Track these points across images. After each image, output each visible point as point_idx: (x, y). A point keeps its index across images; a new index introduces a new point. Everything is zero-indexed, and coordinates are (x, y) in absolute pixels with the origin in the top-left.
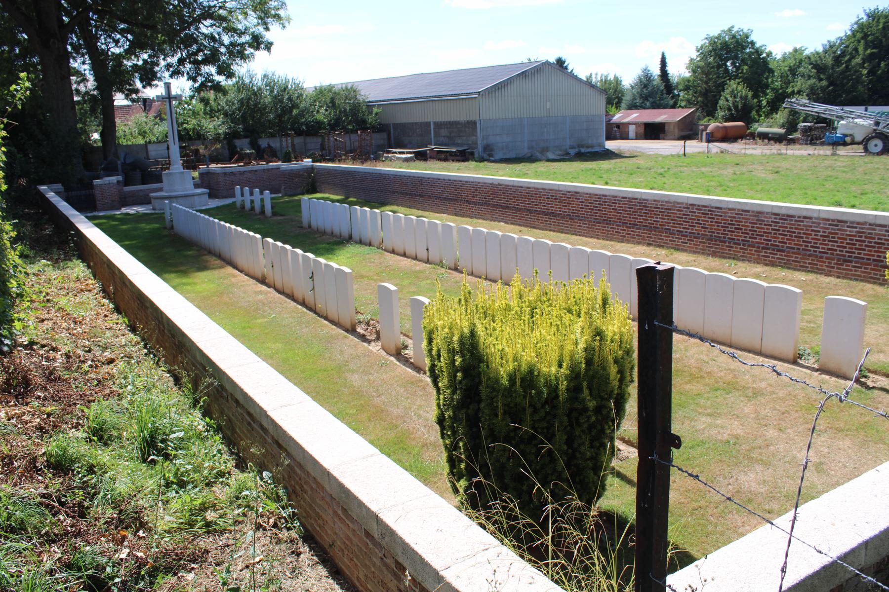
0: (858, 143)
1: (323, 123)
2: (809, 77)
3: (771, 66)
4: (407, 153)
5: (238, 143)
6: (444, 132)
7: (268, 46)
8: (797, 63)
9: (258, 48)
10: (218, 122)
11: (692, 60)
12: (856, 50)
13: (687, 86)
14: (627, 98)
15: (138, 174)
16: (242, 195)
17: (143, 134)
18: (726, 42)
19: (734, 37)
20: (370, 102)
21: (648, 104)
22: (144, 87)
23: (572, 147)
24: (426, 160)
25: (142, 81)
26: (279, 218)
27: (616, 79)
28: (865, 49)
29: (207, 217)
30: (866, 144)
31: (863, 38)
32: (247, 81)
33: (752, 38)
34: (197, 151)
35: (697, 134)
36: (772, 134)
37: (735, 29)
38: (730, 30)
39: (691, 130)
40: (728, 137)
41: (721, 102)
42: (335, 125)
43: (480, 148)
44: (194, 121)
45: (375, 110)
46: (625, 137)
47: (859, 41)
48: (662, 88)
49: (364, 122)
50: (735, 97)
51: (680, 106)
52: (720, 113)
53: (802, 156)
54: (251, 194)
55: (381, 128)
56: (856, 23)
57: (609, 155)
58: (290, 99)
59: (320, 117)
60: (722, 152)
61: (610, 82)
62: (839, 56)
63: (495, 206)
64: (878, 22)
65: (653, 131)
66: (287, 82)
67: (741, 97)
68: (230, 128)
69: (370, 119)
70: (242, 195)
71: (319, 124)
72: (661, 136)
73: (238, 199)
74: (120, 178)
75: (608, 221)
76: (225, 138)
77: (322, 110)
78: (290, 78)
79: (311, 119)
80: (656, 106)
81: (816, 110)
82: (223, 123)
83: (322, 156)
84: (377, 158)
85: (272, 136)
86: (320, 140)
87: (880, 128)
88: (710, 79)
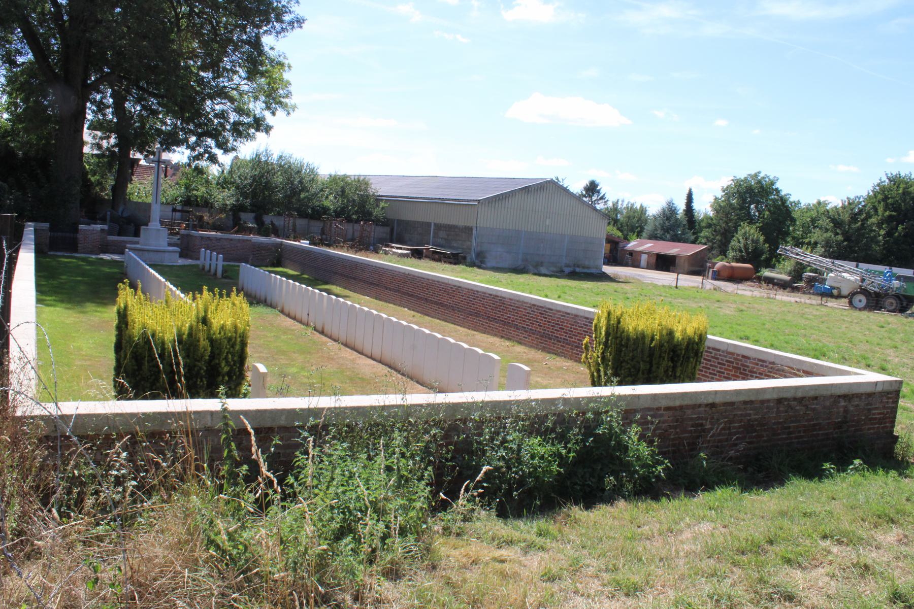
0: (845, 297)
1: (329, 209)
2: (827, 230)
3: (794, 215)
4: (405, 249)
5: (243, 216)
6: (442, 234)
7: (268, 129)
8: (820, 215)
9: (258, 130)
10: (226, 193)
11: (716, 199)
12: (876, 210)
14: (648, 228)
18: (751, 186)
19: (759, 182)
21: (668, 236)
23: (568, 266)
24: (420, 258)
27: (641, 206)
28: (885, 211)
30: (851, 298)
31: (883, 200)
32: (263, 159)
33: (778, 185)
34: (202, 217)
35: (704, 271)
36: (778, 279)
37: (762, 175)
38: (756, 175)
40: (734, 277)
41: (733, 243)
42: (339, 213)
43: (473, 253)
46: (636, 265)
47: (879, 202)
48: (685, 222)
49: (370, 214)
50: (746, 239)
51: (700, 243)
52: (731, 254)
53: (790, 302)
55: (386, 222)
56: (878, 185)
57: (604, 277)
58: (301, 182)
59: (327, 203)
60: (715, 289)
61: (635, 211)
62: (856, 214)
63: (404, 293)
64: (898, 187)
65: (664, 263)
66: (302, 166)
67: (753, 241)
68: (238, 200)
69: (376, 212)
71: (325, 210)
74: (106, 227)
75: (477, 315)
76: (230, 210)
77: (331, 197)
78: (305, 162)
79: (317, 204)
80: (676, 239)
81: (807, 259)
83: (321, 240)
84: (376, 251)
85: (279, 214)
86: (322, 225)
87: (864, 284)
88: (731, 220)
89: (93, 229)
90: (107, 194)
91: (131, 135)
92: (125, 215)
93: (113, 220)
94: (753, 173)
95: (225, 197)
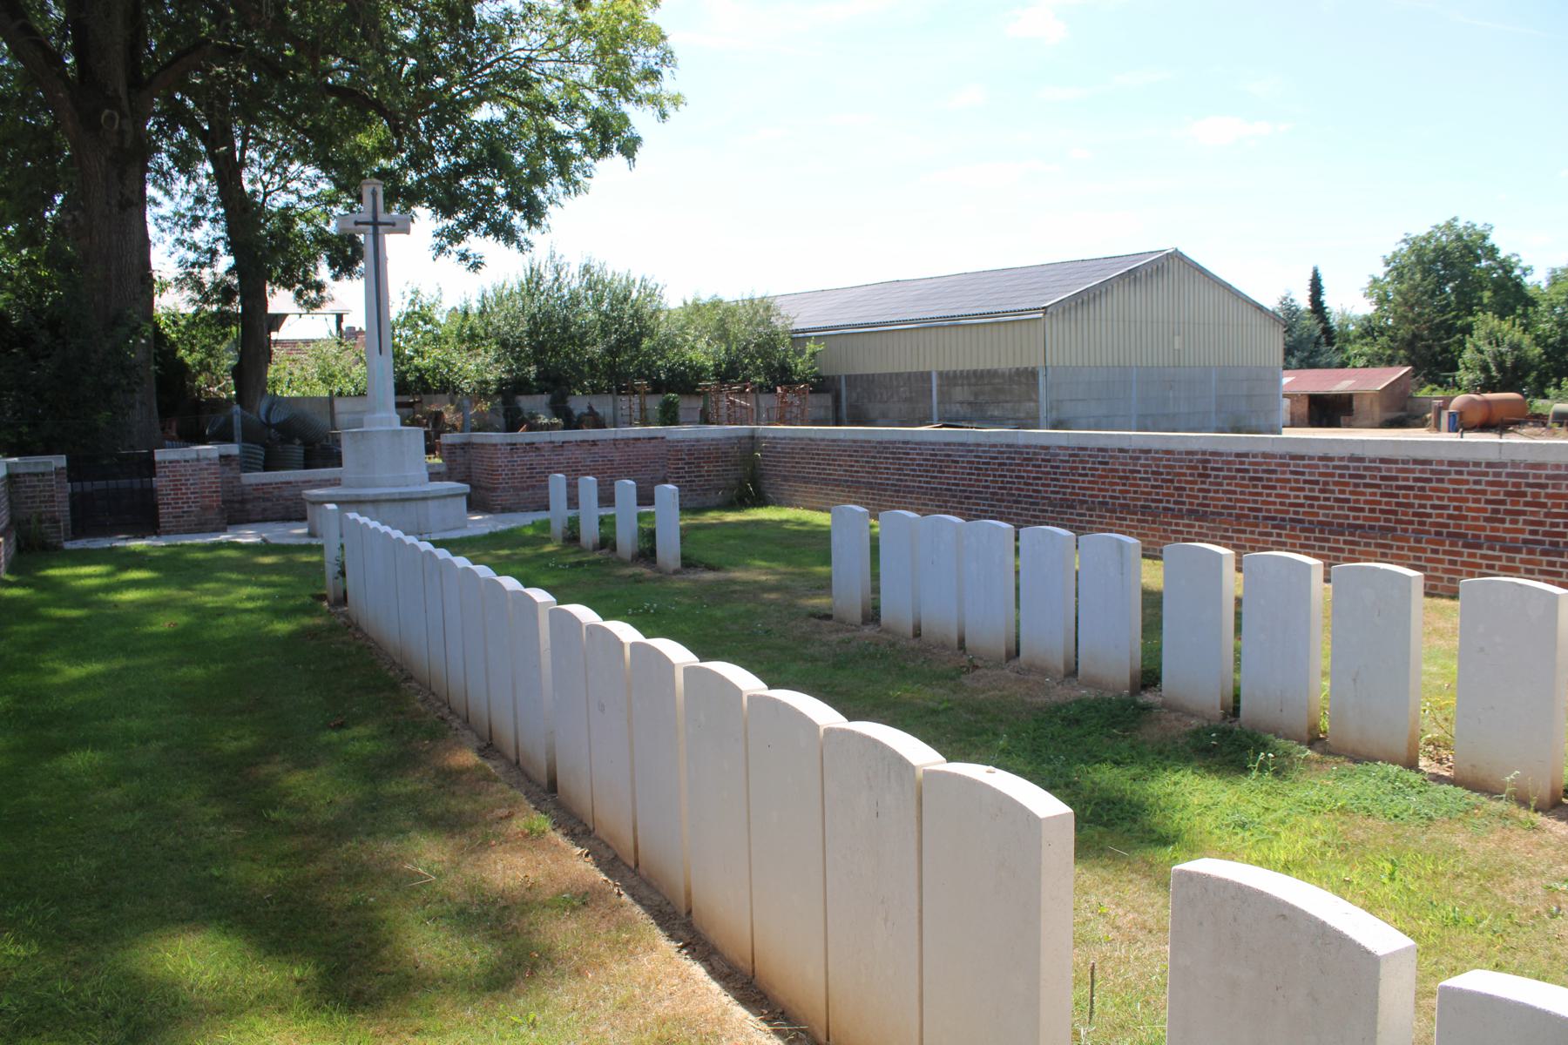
1: (703, 369)
5: (526, 402)
6: (960, 393)
11: (1375, 281)
13: (1369, 330)
15: (297, 450)
16: (573, 501)
17: (327, 379)
19: (1459, 237)
20: (797, 331)
22: (336, 277)
25: (332, 265)
26: (709, 576)
29: (483, 571)
38: (1450, 225)
39: (1403, 409)
41: (1468, 355)
42: (729, 373)
44: (437, 352)
45: (810, 347)
52: (1464, 376)
54: (607, 499)
69: (800, 365)
70: (573, 501)
71: (699, 371)
72: (1343, 419)
73: (559, 513)
74: (233, 449)
76: (498, 392)
77: (701, 345)
78: (636, 275)
82: (497, 361)
85: (596, 390)
89: (189, 463)
90: (224, 388)
91: (265, 252)
92: (276, 418)
93: (249, 436)
94: (1442, 223)
95: (478, 367)
